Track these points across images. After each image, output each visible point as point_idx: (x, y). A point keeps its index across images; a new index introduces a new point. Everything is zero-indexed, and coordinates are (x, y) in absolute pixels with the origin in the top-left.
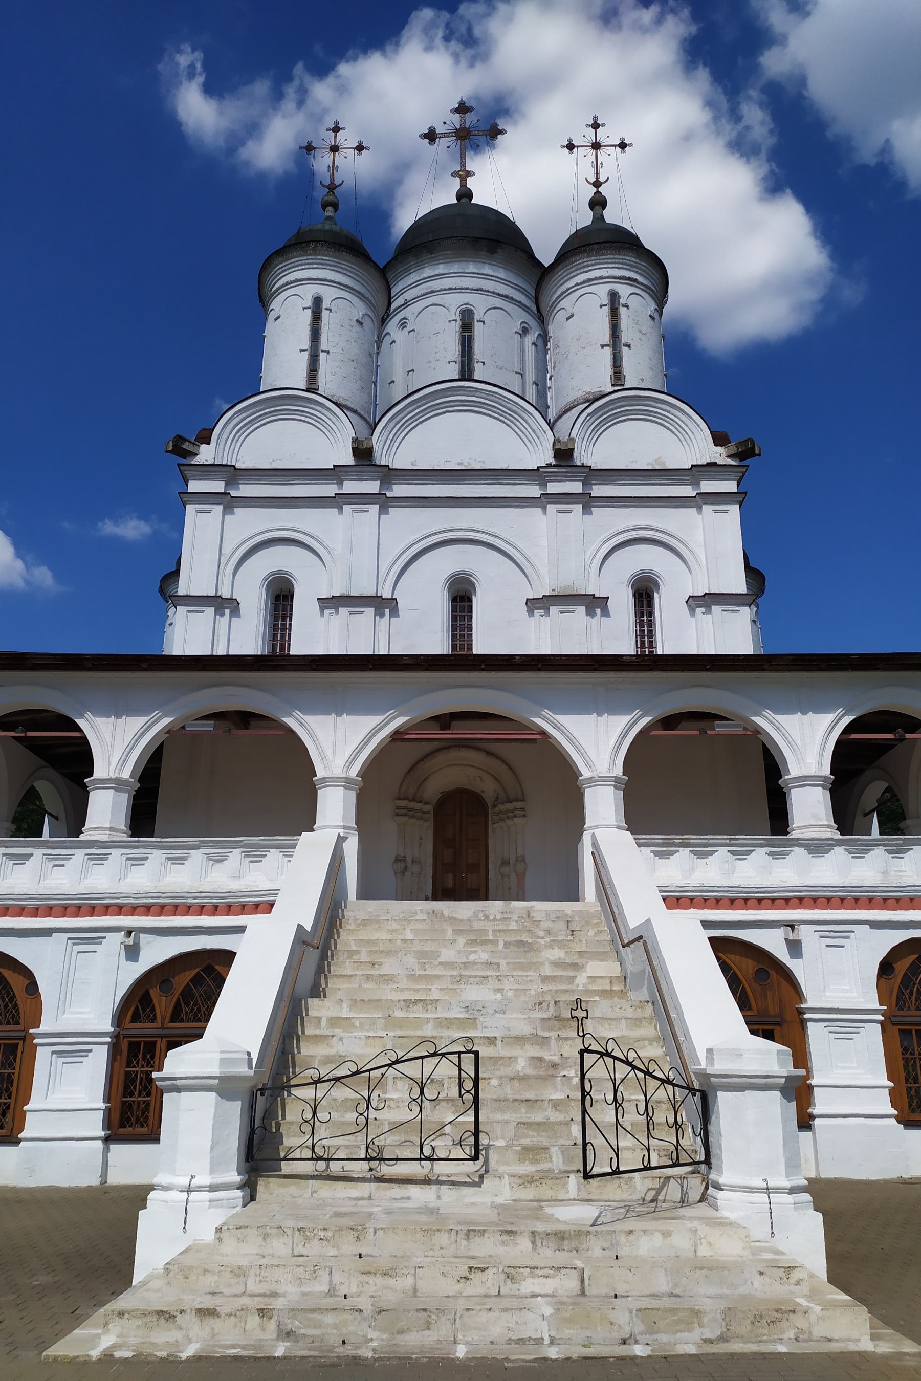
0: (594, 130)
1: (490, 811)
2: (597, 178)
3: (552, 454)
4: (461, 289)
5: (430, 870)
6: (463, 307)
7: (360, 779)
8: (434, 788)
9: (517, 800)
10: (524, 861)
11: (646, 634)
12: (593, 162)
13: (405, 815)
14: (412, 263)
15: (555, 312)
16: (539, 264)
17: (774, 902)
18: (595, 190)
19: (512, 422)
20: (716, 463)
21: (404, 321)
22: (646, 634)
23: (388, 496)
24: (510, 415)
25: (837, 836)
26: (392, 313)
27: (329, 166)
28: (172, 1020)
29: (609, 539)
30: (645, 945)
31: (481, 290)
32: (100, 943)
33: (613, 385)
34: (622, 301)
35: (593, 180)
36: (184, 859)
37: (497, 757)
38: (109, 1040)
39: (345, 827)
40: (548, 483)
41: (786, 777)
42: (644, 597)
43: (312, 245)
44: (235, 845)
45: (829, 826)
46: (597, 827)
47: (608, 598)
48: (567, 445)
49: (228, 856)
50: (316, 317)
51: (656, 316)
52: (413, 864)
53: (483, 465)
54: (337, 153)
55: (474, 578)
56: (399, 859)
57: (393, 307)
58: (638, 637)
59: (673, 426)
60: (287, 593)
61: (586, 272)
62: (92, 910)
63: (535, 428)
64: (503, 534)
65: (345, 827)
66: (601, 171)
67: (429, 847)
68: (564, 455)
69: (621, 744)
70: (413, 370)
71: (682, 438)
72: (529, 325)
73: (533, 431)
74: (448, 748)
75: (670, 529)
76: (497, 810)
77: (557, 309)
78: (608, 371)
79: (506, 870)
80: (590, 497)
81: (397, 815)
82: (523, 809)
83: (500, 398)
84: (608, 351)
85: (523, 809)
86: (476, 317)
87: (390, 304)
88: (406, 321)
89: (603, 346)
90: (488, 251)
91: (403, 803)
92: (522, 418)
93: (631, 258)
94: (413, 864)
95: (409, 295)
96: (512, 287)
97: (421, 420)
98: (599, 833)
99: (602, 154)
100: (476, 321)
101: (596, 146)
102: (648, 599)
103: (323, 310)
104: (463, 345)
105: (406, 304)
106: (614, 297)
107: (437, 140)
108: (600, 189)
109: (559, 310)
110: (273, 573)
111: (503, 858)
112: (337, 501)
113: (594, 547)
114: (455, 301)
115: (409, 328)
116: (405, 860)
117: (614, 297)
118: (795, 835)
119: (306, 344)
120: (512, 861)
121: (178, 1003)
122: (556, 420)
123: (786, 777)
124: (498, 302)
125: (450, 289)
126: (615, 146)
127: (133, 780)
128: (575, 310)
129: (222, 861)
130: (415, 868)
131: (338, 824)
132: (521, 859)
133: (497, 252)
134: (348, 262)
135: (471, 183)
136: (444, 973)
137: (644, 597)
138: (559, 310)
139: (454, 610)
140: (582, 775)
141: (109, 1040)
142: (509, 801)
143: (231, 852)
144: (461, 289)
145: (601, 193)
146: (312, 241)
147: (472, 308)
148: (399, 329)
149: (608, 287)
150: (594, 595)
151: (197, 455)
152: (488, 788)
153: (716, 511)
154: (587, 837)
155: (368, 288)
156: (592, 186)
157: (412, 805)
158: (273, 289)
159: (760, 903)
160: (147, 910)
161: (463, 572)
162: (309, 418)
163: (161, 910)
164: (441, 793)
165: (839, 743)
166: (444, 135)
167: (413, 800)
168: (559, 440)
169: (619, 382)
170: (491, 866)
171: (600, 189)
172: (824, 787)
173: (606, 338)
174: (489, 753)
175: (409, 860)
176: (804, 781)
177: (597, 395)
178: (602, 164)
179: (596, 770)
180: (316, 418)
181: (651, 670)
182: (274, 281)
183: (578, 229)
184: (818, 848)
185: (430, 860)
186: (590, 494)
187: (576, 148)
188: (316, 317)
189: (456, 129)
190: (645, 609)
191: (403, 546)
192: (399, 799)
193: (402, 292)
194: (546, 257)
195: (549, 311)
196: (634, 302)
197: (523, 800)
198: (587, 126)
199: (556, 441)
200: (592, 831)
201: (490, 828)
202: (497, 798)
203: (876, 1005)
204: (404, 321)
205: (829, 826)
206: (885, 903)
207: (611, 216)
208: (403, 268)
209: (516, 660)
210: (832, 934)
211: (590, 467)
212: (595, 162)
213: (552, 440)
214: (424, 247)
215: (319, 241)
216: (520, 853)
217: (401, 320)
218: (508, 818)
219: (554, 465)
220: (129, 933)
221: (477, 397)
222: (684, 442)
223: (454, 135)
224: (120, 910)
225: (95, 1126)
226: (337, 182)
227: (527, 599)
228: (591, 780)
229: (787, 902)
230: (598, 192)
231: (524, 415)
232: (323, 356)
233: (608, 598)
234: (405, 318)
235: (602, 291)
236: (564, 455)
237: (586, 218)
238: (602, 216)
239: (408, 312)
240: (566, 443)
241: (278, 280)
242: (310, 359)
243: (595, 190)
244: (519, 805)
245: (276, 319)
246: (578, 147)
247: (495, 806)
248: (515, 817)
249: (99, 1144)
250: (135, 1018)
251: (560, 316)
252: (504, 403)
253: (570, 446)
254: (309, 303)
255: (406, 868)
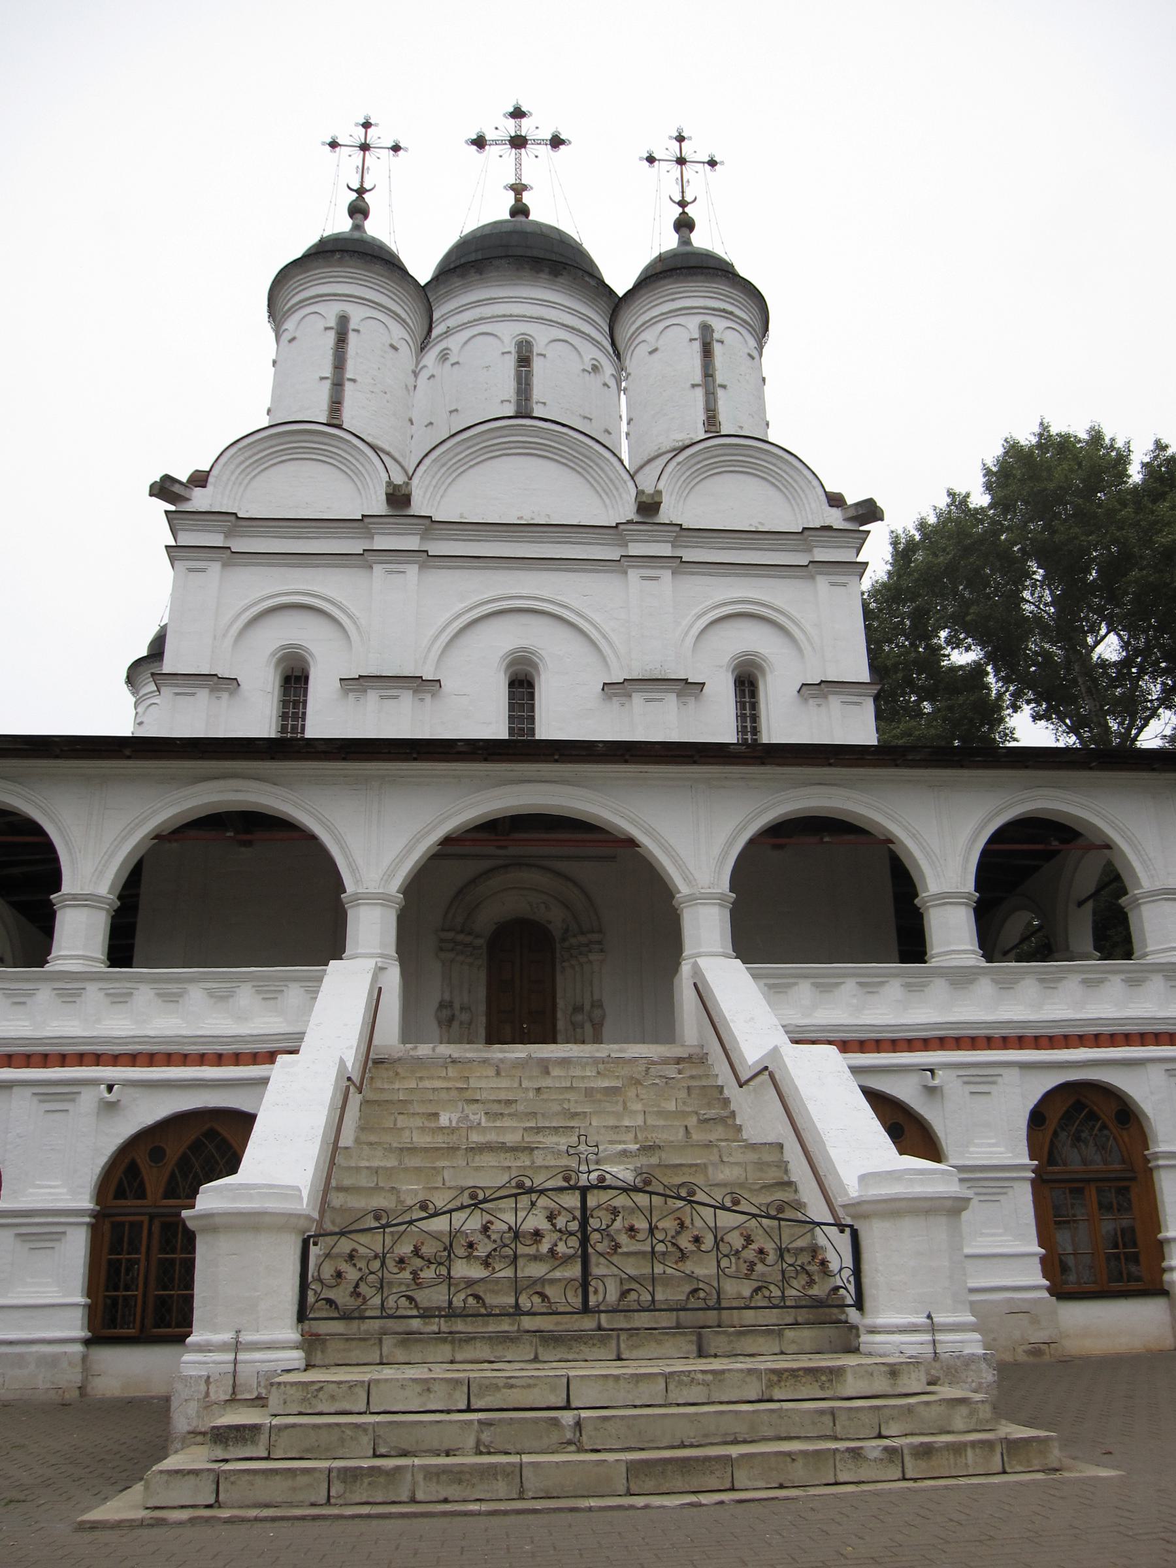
0: (678, 144)
1: (558, 945)
2: (683, 197)
3: (634, 508)
4: (517, 316)
5: (482, 1020)
6: (520, 337)
7: (402, 896)
8: (489, 916)
9: (593, 932)
10: (601, 1006)
11: (749, 730)
12: (677, 179)
13: (452, 950)
14: (457, 285)
15: (634, 345)
16: (611, 292)
17: (910, 1045)
18: (680, 210)
19: (584, 469)
20: (831, 527)
21: (445, 352)
22: (749, 730)
23: (430, 554)
24: (582, 460)
25: (984, 963)
26: (434, 340)
27: (358, 167)
28: (166, 1197)
29: (704, 613)
30: (772, 1076)
31: (542, 319)
32: (73, 1100)
33: (706, 432)
34: (716, 336)
35: (678, 198)
36: (180, 995)
37: (568, 878)
38: (87, 1220)
39: (382, 956)
40: (629, 544)
41: (924, 895)
42: (746, 685)
43: (338, 256)
44: (244, 979)
45: (973, 952)
46: (699, 955)
47: (704, 684)
48: (653, 498)
49: (235, 992)
50: (342, 339)
51: (755, 354)
52: (461, 1012)
53: (548, 520)
54: (367, 153)
55: (537, 657)
56: (442, 1006)
57: (435, 333)
58: (740, 733)
59: (779, 481)
60: (299, 674)
61: (673, 300)
62: (63, 1060)
63: (612, 476)
64: (574, 604)
65: (382, 956)
66: (687, 190)
67: (482, 993)
68: (398, 498)
69: (727, 853)
70: (456, 410)
71: (790, 497)
72: (599, 362)
73: (611, 480)
74: (506, 866)
75: (778, 602)
76: (566, 944)
77: (636, 342)
78: (701, 416)
79: (579, 1018)
80: (681, 562)
81: (441, 949)
82: (600, 943)
83: (569, 440)
84: (699, 393)
85: (600, 943)
86: (536, 350)
87: (430, 330)
88: (448, 352)
89: (694, 386)
90: (550, 273)
91: (450, 935)
92: (597, 465)
93: (725, 289)
94: (461, 1012)
95: (452, 322)
96: (580, 317)
97: (472, 463)
98: (702, 962)
99: (689, 170)
100: (535, 354)
101: (365, 147)
102: (752, 688)
103: (350, 332)
104: (519, 382)
105: (448, 333)
106: (706, 329)
107: (487, 147)
108: (686, 210)
109: (640, 343)
110: (283, 647)
111: (575, 1004)
112: (365, 559)
113: (685, 622)
114: (509, 333)
115: (452, 360)
116: (451, 1006)
117: (706, 329)
118: (933, 963)
119: (328, 371)
120: (587, 1007)
121: (172, 1176)
122: (637, 472)
123: (924, 895)
124: (563, 335)
125: (504, 316)
126: (704, 163)
127: (111, 897)
128: (660, 344)
129: (228, 997)
130: (465, 1017)
131: (375, 951)
132: (597, 1004)
133: (562, 275)
134: (382, 276)
135: (527, 198)
136: (519, 1125)
137: (746, 685)
138: (640, 343)
139: (512, 696)
140: (679, 892)
141: (87, 1220)
142: (583, 933)
143: (239, 986)
144: (517, 316)
145: (687, 214)
146: (338, 251)
147: (529, 338)
148: (439, 361)
149: (698, 319)
150: (687, 679)
151: (188, 499)
152: (555, 918)
153: (833, 584)
154: (686, 968)
155: (406, 307)
156: (677, 206)
157: (460, 937)
158: (287, 307)
159: (894, 1045)
160: (133, 1059)
161: (524, 650)
162: (331, 457)
163: (151, 1059)
164: (496, 924)
165: (984, 854)
166: (496, 143)
167: (462, 932)
168: (643, 492)
169: (713, 429)
170: (559, 1015)
171: (686, 210)
172: (966, 904)
173: (698, 377)
174: (558, 874)
175: (457, 1006)
176: (945, 898)
177: (687, 442)
178: (688, 181)
179: (697, 885)
180: (340, 459)
181: (763, 764)
182: (289, 297)
183: (662, 252)
184: (961, 978)
185: (482, 1008)
186: (681, 557)
187: (657, 162)
188: (342, 339)
189: (511, 137)
190: (747, 700)
191: (447, 615)
192: (443, 930)
193: (444, 318)
194: (620, 280)
195: (626, 345)
196: (731, 337)
197: (600, 931)
198: (671, 138)
199: (640, 493)
200: (693, 960)
201: (558, 968)
202: (567, 930)
203: (1026, 1160)
204: (445, 352)
205: (973, 952)
206: (1038, 1042)
207: (700, 240)
208: (445, 290)
209: (598, 749)
210: (972, 1079)
211: (681, 525)
212: (680, 179)
213: (633, 492)
214: (472, 266)
215: (347, 251)
216: (596, 997)
217: (441, 351)
218: (581, 954)
219: (637, 522)
220: (110, 1088)
221: (541, 438)
222: (793, 502)
223: (507, 142)
224: (98, 1059)
225: (74, 1327)
226: (367, 186)
227: (604, 684)
228: (692, 898)
229: (926, 1044)
230: (684, 213)
231: (599, 462)
232: (348, 386)
233: (704, 684)
234: (445, 349)
235: (693, 324)
236: (398, 498)
237: (670, 241)
238: (689, 239)
239: (454, 342)
240: (652, 496)
241: (297, 293)
242: (333, 389)
243: (680, 210)
244: (595, 937)
245: (290, 341)
246: (659, 160)
247: (564, 940)
248: (590, 952)
249: (79, 1348)
250: (120, 1194)
251: (642, 350)
252: (575, 446)
253: (657, 499)
254: (332, 323)
255: (453, 1016)
